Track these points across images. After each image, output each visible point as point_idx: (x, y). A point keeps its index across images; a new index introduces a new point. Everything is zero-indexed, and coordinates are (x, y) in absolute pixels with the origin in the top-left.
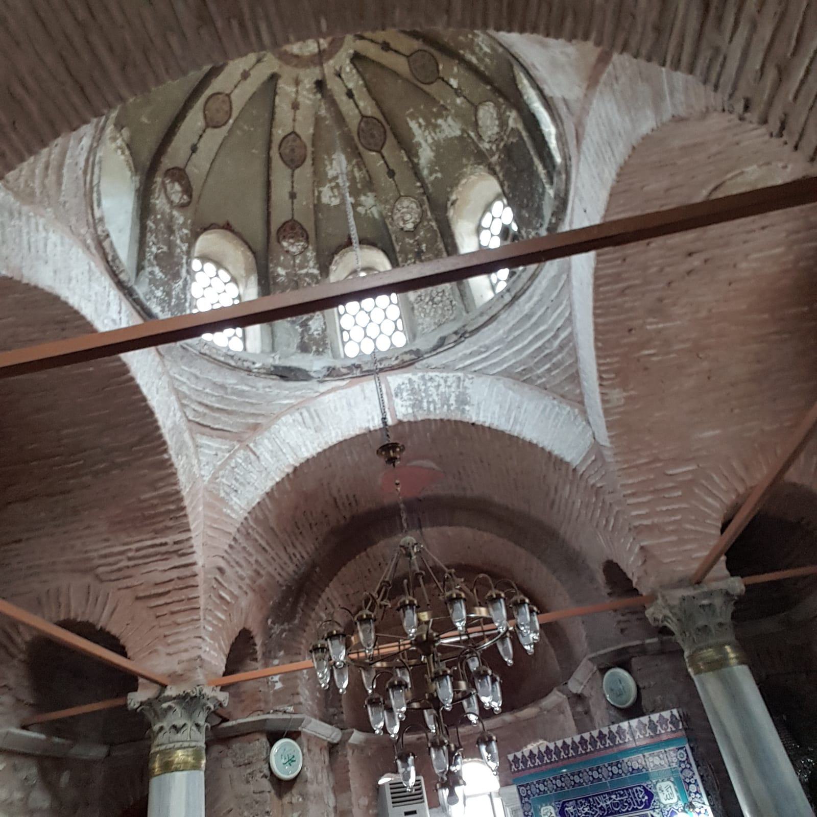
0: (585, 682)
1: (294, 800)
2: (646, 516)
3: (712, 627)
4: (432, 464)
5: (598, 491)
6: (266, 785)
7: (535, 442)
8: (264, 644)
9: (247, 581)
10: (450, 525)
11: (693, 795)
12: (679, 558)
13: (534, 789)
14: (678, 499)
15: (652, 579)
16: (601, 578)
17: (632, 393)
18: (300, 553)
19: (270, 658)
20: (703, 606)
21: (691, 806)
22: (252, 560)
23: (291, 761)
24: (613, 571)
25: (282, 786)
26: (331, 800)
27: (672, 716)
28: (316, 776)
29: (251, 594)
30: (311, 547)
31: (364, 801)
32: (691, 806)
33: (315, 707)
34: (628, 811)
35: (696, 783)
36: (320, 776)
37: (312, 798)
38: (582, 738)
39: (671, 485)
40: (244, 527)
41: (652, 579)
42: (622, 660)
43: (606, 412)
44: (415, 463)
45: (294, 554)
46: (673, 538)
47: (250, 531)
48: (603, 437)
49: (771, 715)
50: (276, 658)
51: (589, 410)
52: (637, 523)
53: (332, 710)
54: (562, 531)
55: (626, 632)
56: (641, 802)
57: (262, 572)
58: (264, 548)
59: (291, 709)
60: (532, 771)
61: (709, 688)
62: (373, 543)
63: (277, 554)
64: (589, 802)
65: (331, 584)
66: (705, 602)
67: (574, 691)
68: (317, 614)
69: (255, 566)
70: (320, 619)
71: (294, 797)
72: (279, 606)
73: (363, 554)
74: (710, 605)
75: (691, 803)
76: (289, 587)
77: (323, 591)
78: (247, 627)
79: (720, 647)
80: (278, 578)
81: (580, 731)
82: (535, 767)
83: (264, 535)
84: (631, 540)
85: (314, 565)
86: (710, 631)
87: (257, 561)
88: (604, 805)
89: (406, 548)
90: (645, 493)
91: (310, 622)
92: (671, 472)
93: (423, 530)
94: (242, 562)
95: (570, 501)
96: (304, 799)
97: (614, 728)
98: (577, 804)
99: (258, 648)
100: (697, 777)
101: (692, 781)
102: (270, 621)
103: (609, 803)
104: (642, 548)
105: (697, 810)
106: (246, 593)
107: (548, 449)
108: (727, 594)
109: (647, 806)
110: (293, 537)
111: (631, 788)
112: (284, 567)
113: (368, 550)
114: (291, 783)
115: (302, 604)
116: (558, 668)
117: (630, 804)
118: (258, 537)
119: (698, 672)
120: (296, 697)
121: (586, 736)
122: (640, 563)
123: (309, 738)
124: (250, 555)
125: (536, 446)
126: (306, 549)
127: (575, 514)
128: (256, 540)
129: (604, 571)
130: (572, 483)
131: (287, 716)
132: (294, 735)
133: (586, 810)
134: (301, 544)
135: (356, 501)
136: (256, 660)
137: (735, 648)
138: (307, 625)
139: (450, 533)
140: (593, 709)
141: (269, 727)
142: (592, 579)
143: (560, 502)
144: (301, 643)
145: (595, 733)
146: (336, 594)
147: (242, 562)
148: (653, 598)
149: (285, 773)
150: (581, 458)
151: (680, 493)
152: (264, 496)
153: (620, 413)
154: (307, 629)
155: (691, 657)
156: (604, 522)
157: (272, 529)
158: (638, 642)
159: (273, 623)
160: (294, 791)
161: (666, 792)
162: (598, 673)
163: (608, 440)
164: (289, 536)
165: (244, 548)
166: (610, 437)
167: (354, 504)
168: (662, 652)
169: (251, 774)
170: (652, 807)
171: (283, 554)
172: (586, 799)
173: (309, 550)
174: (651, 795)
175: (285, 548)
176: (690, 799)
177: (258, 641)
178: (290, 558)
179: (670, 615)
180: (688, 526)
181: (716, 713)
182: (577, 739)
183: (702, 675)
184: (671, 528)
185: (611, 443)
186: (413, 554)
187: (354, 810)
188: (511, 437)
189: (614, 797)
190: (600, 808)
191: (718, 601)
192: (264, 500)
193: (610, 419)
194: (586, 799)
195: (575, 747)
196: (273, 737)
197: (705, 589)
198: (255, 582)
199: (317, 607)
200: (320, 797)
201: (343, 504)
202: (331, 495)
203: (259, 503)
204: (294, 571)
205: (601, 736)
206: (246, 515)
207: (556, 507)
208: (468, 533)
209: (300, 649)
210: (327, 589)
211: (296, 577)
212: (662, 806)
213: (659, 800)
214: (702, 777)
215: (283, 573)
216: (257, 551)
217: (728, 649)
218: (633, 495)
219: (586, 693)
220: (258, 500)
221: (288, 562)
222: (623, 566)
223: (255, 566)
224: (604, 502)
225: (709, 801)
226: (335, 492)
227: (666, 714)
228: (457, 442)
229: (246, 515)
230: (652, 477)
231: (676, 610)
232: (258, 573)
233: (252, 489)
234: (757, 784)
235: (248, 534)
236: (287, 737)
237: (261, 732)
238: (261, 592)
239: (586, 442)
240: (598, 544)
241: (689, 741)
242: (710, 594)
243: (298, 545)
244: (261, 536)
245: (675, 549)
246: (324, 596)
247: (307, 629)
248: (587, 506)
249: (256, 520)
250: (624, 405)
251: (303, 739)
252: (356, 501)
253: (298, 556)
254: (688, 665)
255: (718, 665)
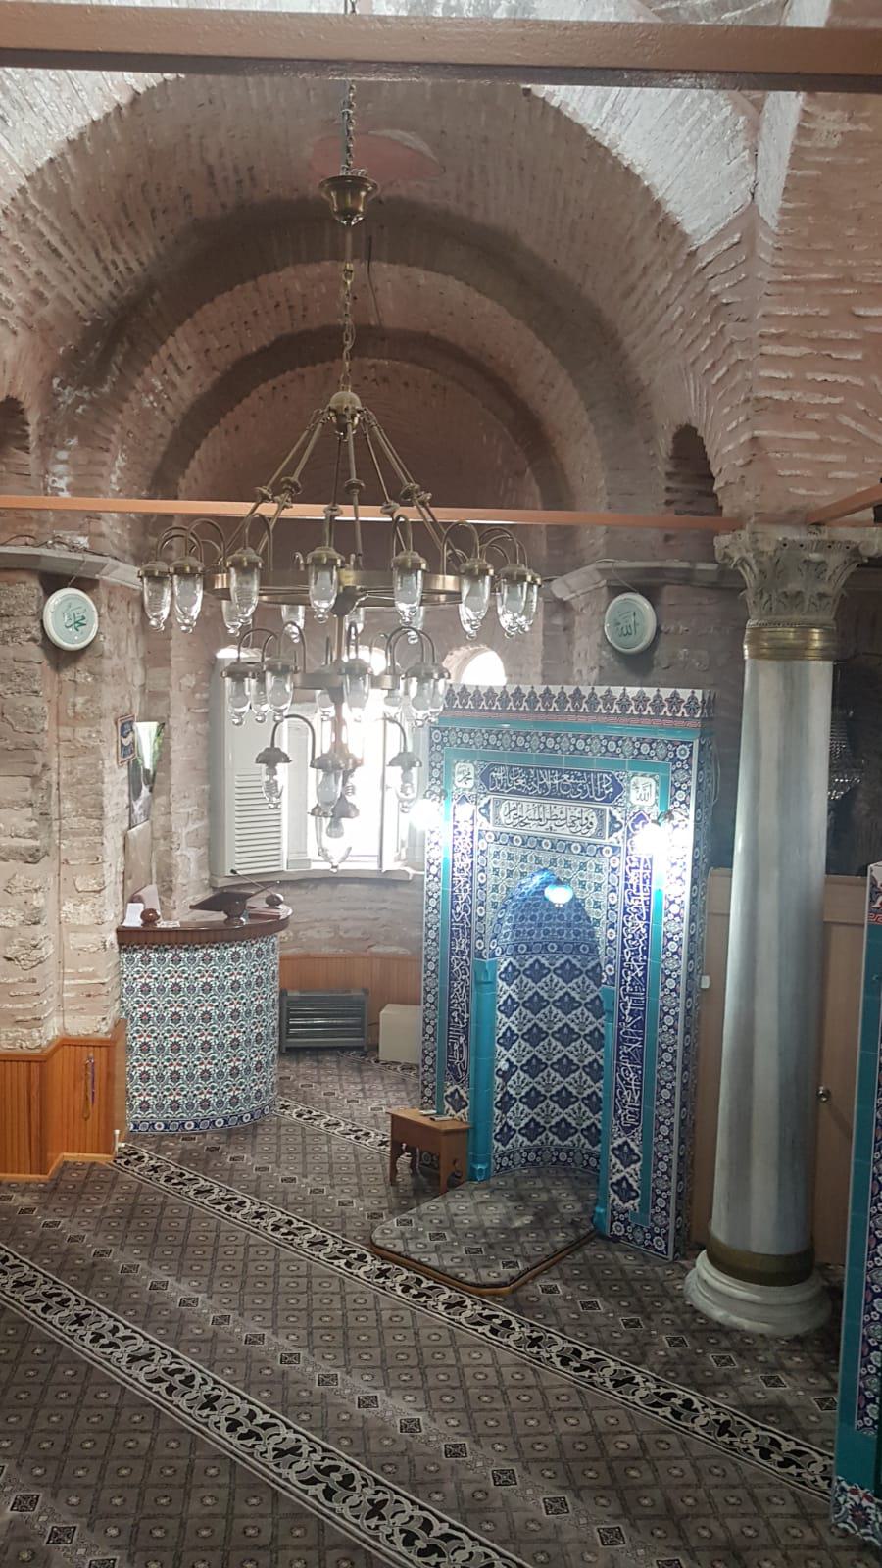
0: (579, 592)
1: (80, 679)
2: (784, 384)
3: (807, 596)
4: (425, 148)
5: (719, 309)
6: (35, 652)
7: (638, 171)
8: (43, 422)
9: (18, 311)
10: (428, 268)
11: (677, 804)
12: (808, 473)
13: (452, 738)
14: (856, 367)
15: (749, 495)
16: (665, 445)
17: (863, 127)
18: (126, 261)
19: (51, 445)
20: (808, 562)
21: (669, 815)
22: (30, 272)
23: (80, 624)
24: (690, 450)
25: (61, 657)
26: (137, 676)
27: (692, 698)
28: (118, 647)
29: (23, 335)
30: (148, 250)
31: (190, 681)
32: (669, 815)
33: (126, 536)
34: (579, 798)
35: (688, 791)
36: (123, 645)
37: (109, 679)
38: (547, 691)
39: (851, 336)
40: (18, 208)
41: (749, 495)
42: (649, 586)
43: (797, 157)
44: (387, 133)
45: (114, 262)
46: (813, 436)
47: (29, 215)
48: (771, 203)
49: (833, 705)
50: (63, 448)
51: (765, 130)
52: (762, 394)
53: (153, 540)
54: (628, 341)
55: (672, 542)
56: (602, 794)
57: (47, 294)
58: (55, 251)
59: (84, 541)
60: (459, 714)
61: (762, 683)
62: (273, 268)
63: (79, 260)
64: (529, 774)
65: (179, 332)
66: (815, 556)
67: (559, 596)
68: (146, 382)
69: (35, 284)
70: (151, 389)
71: (81, 674)
72: (75, 356)
73: (250, 285)
74: (822, 563)
75: (670, 813)
76: (96, 322)
77: (163, 342)
78: (13, 394)
79: (805, 629)
80: (79, 306)
81: (546, 679)
82: (464, 709)
83: (57, 225)
84: (741, 419)
85: (150, 286)
86: (803, 601)
87: (39, 274)
88: (549, 783)
89: (340, 416)
90: (797, 340)
91: (132, 396)
92: (862, 312)
93: (374, 263)
94: (11, 276)
95: (662, 303)
96: (95, 680)
97: (600, 691)
98: (510, 772)
99: (31, 430)
100: (693, 784)
101: (684, 787)
102: (56, 382)
103: (556, 782)
104: (754, 439)
105: (675, 822)
106: (15, 333)
107: (658, 195)
108: (856, 551)
109: (608, 800)
110: (116, 233)
111: (595, 773)
112: (90, 284)
113: (260, 279)
114: (76, 656)
115: (119, 358)
116: (544, 553)
117: (585, 792)
118: (45, 229)
119: (757, 655)
120: (94, 522)
121: (555, 690)
122: (740, 462)
123: (112, 589)
124: (27, 261)
125: (638, 179)
126: (136, 257)
127: (661, 328)
128: (42, 235)
129: (676, 437)
130: (678, 273)
131: (79, 557)
132: (87, 584)
133: (521, 782)
134: (129, 244)
135: (252, 179)
136: (26, 449)
137: (827, 634)
138: (126, 400)
139: (422, 282)
140: (578, 632)
141: (44, 566)
142: (649, 440)
143: (645, 293)
144: (113, 432)
145: (569, 690)
146: (185, 347)
147: (11, 276)
148: (736, 525)
149: (68, 640)
150: (712, 234)
151: (859, 356)
152: (64, 146)
153: (818, 165)
154: (126, 406)
155: (756, 630)
156: (708, 366)
157: (75, 214)
158: (685, 565)
159: (62, 384)
160: (81, 666)
161: (641, 790)
162: (604, 591)
163: (777, 216)
164: (108, 229)
165: (16, 248)
166: (783, 211)
167: (247, 183)
168: (714, 587)
169: (11, 631)
170: (615, 802)
171: (90, 260)
172: (526, 769)
173: (144, 259)
174: (619, 789)
175: (97, 254)
176: (671, 807)
177: (33, 417)
178: (106, 269)
179: (753, 562)
180: (845, 420)
181: (756, 715)
182: (540, 690)
183: (761, 662)
184: (816, 416)
185: (781, 224)
186: (350, 427)
187: (172, 694)
188: (595, 145)
189: (566, 777)
190: (541, 786)
191: (835, 559)
192: (62, 155)
193: (799, 173)
194: (526, 769)
195: (532, 699)
196: (53, 582)
197: (825, 537)
198: (32, 313)
199: (147, 371)
200: (120, 675)
201: (226, 180)
202: (203, 160)
203: (51, 160)
204: (111, 294)
205: (577, 696)
206: (23, 182)
207: (634, 297)
208: (455, 289)
209: (109, 441)
210: (170, 340)
211: (114, 304)
212: (629, 805)
213: (628, 798)
214: (699, 785)
215: (90, 298)
216: (40, 254)
217: (816, 634)
218: (778, 338)
219: (578, 604)
220: (50, 154)
221: (102, 278)
222: (710, 451)
223: (35, 284)
224: (721, 332)
225: (696, 815)
226: (212, 157)
227: (685, 694)
228: (483, 117)
229: (23, 182)
230: (825, 312)
231: (765, 558)
232: (39, 296)
233: (39, 123)
234: (770, 820)
235: (25, 220)
236: (76, 585)
237: (30, 571)
238: (43, 331)
239: (732, 201)
240: (682, 391)
241: (701, 737)
242: (830, 545)
243: (124, 248)
244: (52, 226)
245: (808, 456)
246: (163, 351)
247: (126, 406)
248: (689, 325)
249: (44, 195)
250: (838, 149)
251: (102, 592)
252: (252, 179)
253: (122, 267)
254: (746, 640)
255: (789, 654)
